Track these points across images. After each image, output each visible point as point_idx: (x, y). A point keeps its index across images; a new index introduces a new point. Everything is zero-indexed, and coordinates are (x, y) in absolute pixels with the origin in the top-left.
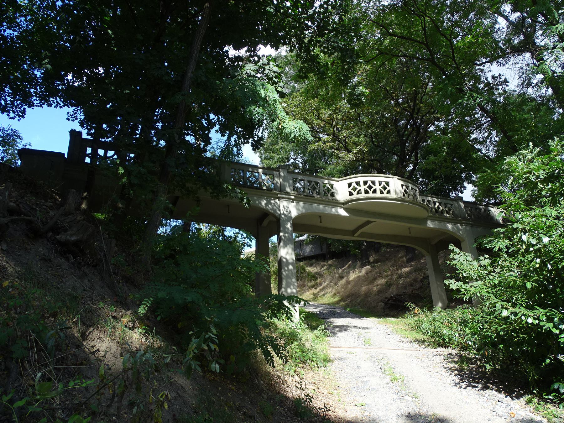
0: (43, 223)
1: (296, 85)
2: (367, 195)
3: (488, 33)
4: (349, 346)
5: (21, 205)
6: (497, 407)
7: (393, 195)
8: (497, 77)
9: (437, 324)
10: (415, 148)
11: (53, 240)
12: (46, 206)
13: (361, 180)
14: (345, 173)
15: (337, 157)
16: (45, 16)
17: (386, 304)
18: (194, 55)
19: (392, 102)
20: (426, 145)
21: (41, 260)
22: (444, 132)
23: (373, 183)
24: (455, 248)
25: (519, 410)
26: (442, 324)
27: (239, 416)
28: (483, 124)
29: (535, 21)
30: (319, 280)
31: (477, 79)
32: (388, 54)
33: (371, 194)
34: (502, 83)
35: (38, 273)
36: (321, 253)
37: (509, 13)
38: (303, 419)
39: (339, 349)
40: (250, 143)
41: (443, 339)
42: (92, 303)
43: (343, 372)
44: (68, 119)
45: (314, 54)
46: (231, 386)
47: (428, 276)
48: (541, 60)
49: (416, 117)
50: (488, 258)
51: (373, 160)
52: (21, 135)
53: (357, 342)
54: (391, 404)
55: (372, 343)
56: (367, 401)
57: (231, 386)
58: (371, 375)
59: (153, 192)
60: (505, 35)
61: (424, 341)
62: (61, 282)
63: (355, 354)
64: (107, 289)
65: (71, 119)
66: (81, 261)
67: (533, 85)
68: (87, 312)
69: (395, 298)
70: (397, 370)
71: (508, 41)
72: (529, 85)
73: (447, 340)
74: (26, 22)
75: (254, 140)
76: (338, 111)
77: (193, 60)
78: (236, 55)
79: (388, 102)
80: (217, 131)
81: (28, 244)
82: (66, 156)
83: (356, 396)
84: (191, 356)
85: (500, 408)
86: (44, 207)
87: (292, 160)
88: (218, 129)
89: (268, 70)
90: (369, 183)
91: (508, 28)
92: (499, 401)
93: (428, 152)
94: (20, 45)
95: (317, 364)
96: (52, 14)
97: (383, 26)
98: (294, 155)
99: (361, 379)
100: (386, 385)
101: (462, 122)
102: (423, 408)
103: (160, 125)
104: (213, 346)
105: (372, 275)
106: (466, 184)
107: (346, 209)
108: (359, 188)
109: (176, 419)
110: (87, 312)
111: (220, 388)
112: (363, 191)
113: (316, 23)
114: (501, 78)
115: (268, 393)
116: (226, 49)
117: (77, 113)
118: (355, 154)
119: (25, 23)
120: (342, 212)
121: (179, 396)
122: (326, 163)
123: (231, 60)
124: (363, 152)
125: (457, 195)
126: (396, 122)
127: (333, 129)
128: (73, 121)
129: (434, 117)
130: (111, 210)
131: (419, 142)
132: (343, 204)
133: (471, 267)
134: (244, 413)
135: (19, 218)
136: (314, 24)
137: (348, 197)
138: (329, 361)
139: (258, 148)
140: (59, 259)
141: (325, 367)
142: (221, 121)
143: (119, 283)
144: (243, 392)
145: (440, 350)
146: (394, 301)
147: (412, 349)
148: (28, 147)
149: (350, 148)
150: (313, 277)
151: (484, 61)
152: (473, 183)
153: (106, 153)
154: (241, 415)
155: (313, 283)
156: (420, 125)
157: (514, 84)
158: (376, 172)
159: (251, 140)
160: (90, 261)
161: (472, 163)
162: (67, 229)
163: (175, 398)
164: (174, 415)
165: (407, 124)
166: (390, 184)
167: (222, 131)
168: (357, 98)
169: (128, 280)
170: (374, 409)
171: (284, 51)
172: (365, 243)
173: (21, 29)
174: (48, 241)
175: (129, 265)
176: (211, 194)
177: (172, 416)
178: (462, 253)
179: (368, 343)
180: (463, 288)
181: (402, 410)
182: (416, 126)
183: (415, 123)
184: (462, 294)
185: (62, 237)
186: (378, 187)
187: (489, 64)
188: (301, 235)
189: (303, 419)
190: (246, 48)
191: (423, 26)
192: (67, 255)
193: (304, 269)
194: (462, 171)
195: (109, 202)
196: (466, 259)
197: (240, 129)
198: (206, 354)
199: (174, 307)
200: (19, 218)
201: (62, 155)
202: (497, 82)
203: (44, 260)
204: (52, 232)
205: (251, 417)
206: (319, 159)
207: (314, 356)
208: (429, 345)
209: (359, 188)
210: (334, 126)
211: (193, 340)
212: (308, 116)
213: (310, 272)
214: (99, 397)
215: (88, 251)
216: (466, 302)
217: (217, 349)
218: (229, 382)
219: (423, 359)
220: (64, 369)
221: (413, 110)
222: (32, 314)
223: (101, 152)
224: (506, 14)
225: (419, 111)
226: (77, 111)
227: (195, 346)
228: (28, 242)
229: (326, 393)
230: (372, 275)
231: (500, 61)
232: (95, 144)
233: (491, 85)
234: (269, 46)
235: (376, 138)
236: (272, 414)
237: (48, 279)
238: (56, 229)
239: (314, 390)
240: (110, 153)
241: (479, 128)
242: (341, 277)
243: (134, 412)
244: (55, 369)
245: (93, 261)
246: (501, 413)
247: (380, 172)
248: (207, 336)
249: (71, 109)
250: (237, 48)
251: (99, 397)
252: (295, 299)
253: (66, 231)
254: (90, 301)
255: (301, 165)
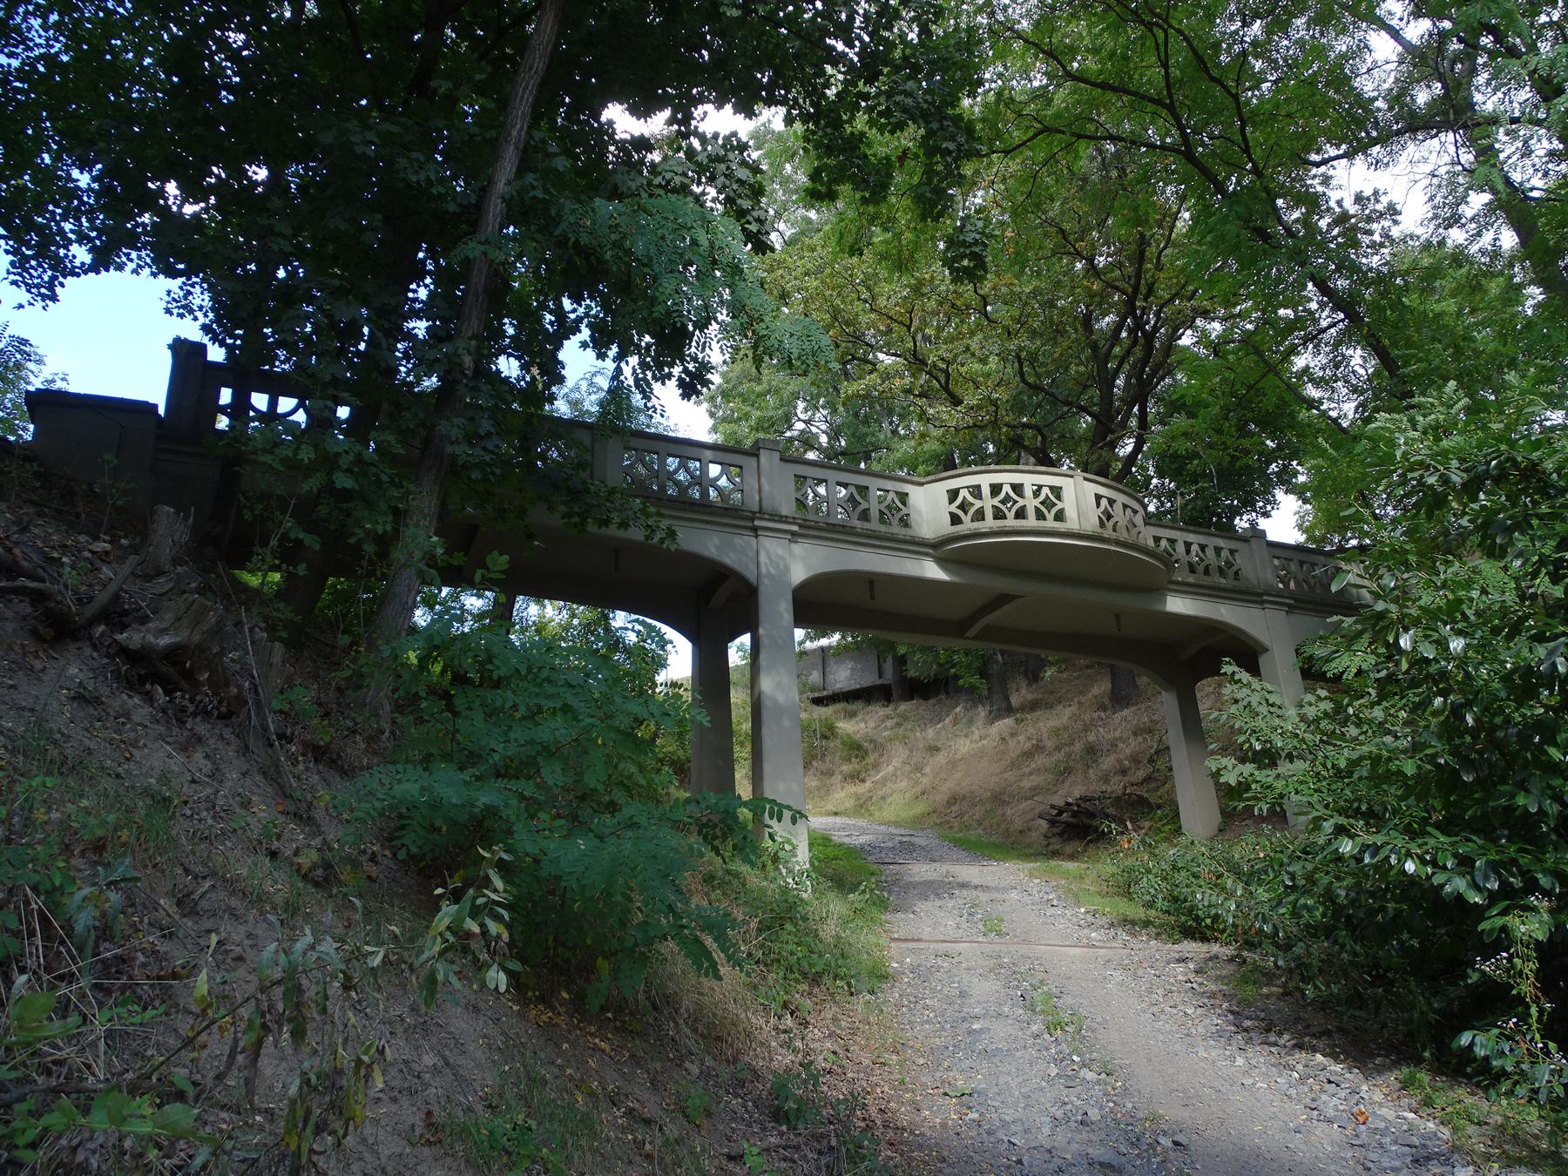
0: (80, 600)
1: (813, 215)
2: (1000, 523)
3: (1340, 79)
4: (942, 938)
5: (17, 551)
6: (1324, 1097)
7: (1072, 523)
8: (1368, 199)
9: (1181, 877)
10: (1140, 392)
11: (109, 646)
12: (91, 551)
13: (985, 481)
14: (946, 464)
15: (923, 416)
16: (101, 14)
17: (1052, 823)
18: (514, 133)
19: (1079, 266)
20: (1170, 385)
21: (74, 698)
22: (1217, 348)
23: (1017, 488)
24: (1237, 669)
25: (1381, 1105)
26: (1196, 876)
27: (615, 1118)
28: (1324, 330)
29: (1472, 47)
30: (871, 758)
31: (1313, 203)
32: (1063, 133)
33: (1011, 522)
34: (1381, 215)
35: (63, 735)
36: (879, 682)
37: (1401, 19)
38: (796, 1129)
39: (915, 945)
40: (674, 379)
41: (1197, 919)
42: (214, 818)
43: (919, 1007)
44: (168, 311)
45: (852, 133)
46: (597, 1041)
47: (1168, 748)
48: (1487, 154)
49: (1143, 309)
50: (1326, 698)
51: (1025, 426)
52: (39, 351)
53: (964, 925)
54: (1041, 1089)
55: (1004, 927)
56: (978, 1081)
57: (597, 1041)
58: (994, 1014)
59: (396, 512)
60: (1391, 80)
61: (1147, 924)
62: (128, 759)
63: (957, 959)
64: (259, 778)
65: (175, 311)
66: (186, 703)
67: (1463, 221)
68: (196, 840)
69: (1079, 806)
70: (1068, 1000)
71: (1399, 97)
72: (1454, 220)
73: (1208, 921)
74: (46, 32)
75: (685, 370)
76: (925, 290)
77: (512, 148)
78: (637, 134)
79: (1067, 265)
80: (584, 345)
81: (38, 657)
82: (161, 411)
83: (949, 1069)
84: (437, 948)
85: (1332, 1102)
86: (87, 554)
87: (800, 426)
88: (588, 339)
89: (723, 178)
90: (1007, 489)
91: (1400, 63)
92: (1330, 1082)
93: (1176, 406)
94: (28, 97)
95: (849, 985)
96: (121, 10)
97: (1051, 54)
98: (806, 410)
99: (966, 1025)
100: (1031, 1041)
101: (1267, 322)
102: (1126, 1101)
103: (420, 327)
104: (494, 928)
105: (1019, 743)
106: (1279, 494)
107: (942, 562)
108: (978, 504)
109: (432, 1125)
110: (196, 840)
111: (565, 1046)
112: (989, 514)
113: (857, 43)
114: (1378, 201)
115: (702, 1062)
116: (606, 116)
117: (191, 293)
118: (972, 408)
119: (43, 34)
120: (932, 571)
121: (448, 1064)
122: (895, 432)
123: (621, 145)
124: (994, 403)
125: (1253, 524)
126: (1087, 321)
127: (914, 338)
128: (181, 316)
129: (1194, 310)
130: (277, 562)
131: (1151, 377)
132: (936, 548)
133: (1277, 722)
134: (630, 1112)
135: (10, 584)
136: (852, 47)
137: (946, 528)
138: (884, 977)
139: (698, 393)
140: (124, 696)
141: (872, 992)
142: (596, 317)
143: (295, 763)
144: (632, 1056)
145: (1190, 947)
146: (1074, 815)
147: (1114, 945)
148: (59, 385)
149: (958, 391)
150: (856, 749)
151: (1333, 152)
152: (1299, 491)
153: (273, 404)
154: (621, 1117)
155: (854, 765)
156: (1156, 329)
157: (1414, 219)
158: (1032, 460)
159: (677, 370)
160: (211, 702)
161: (1298, 436)
162: (148, 616)
163: (435, 1070)
164: (429, 1114)
165: (1119, 327)
166: (1065, 494)
167: (599, 344)
168: (968, 252)
169: (319, 754)
170: (996, 1104)
171: (773, 117)
172: (1000, 657)
173: (31, 49)
174: (94, 647)
175: (327, 715)
176: (563, 517)
177: (423, 1116)
178: (1256, 684)
179: (994, 928)
180: (1257, 782)
181: (1069, 1107)
182: (1144, 332)
183: (1139, 324)
184: (1248, 799)
185: (132, 638)
186: (1031, 503)
187: (1344, 161)
188: (817, 637)
189: (796, 1129)
190: (667, 113)
191: (1162, 54)
192: (148, 687)
193: (831, 728)
194: (1270, 457)
195: (274, 542)
196: (1267, 700)
197: (648, 338)
198: (475, 945)
199: (444, 829)
200: (10, 584)
201: (148, 408)
202: (1367, 212)
203: (81, 698)
204: (107, 625)
205: (648, 1122)
206: (875, 421)
207: (840, 962)
208: (1158, 934)
209: (978, 504)
210: (916, 332)
211: (444, 908)
212: (843, 302)
213: (849, 736)
214: (195, 1054)
215: (206, 675)
216: (1262, 819)
217: (505, 936)
218: (593, 1029)
219: (1140, 972)
220: (123, 988)
221: (1136, 288)
222: (39, 843)
223: (260, 401)
224: (1394, 23)
225: (1151, 290)
226: (193, 286)
227: (447, 921)
228: (37, 652)
229: (867, 1062)
230: (1019, 743)
231: (1375, 155)
232: (243, 373)
233: (1353, 220)
234: (728, 108)
235: (1031, 364)
236: (709, 1115)
237: (90, 751)
238: (116, 615)
239: (834, 1053)
240: (286, 404)
241: (1313, 338)
242: (933, 749)
243: (290, 1092)
244: (97, 987)
245: (220, 702)
246: (1331, 1113)
247: (1044, 460)
248: (481, 901)
249: (175, 284)
250: (642, 110)
251: (195, 1054)
252: (768, 806)
253: (144, 620)
254: (208, 810)
255: (824, 439)
